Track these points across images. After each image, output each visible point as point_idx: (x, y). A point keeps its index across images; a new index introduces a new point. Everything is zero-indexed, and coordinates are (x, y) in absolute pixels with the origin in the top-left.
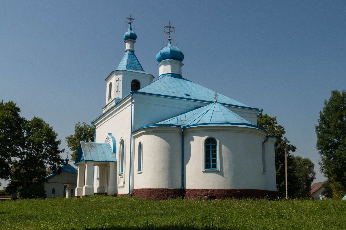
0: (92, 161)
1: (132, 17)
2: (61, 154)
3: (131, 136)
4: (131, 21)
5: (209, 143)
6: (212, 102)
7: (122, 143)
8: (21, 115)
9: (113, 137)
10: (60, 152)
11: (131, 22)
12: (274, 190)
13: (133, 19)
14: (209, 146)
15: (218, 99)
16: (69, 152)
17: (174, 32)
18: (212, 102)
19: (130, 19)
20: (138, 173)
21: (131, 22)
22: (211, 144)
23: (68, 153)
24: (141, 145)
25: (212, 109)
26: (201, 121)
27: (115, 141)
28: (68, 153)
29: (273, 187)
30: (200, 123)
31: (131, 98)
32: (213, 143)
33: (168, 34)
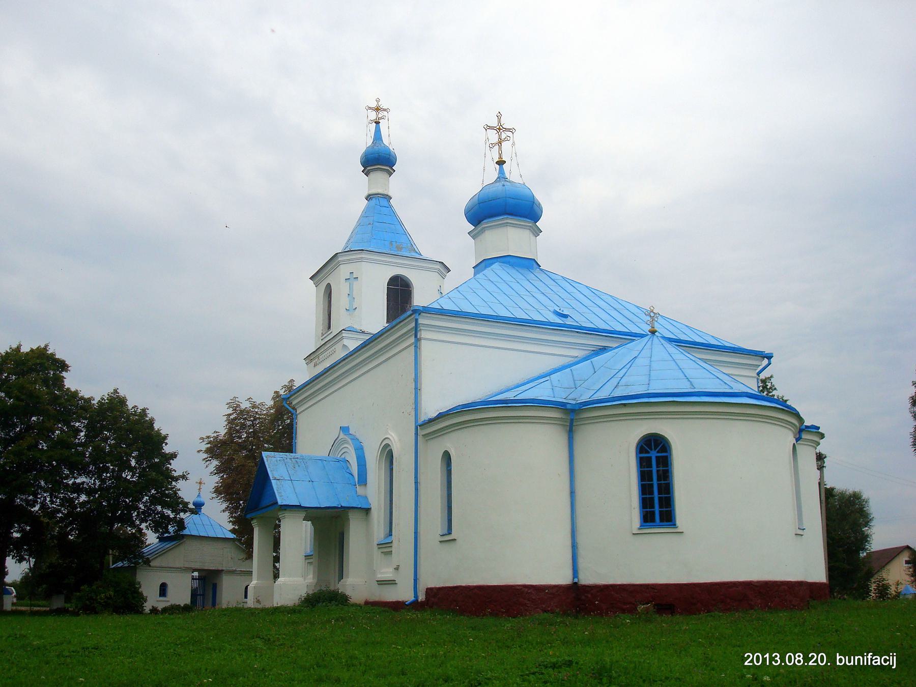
0: (299, 507)
1: (383, 105)
2: (180, 484)
3: (416, 434)
4: (380, 116)
5: (647, 452)
6: (642, 336)
7: (388, 455)
8: (71, 382)
9: (355, 439)
10: (176, 479)
11: (382, 118)
12: (810, 579)
13: (385, 110)
14: (650, 459)
15: (657, 327)
16: (204, 480)
17: (511, 141)
18: (642, 336)
19: (377, 109)
20: (441, 542)
21: (382, 118)
22: (653, 454)
23: (200, 483)
24: (392, 456)
25: (646, 352)
26: (620, 388)
27: (362, 448)
28: (200, 483)
29: (818, 573)
30: (618, 393)
31: (413, 324)
32: (658, 452)
33: (497, 147)
